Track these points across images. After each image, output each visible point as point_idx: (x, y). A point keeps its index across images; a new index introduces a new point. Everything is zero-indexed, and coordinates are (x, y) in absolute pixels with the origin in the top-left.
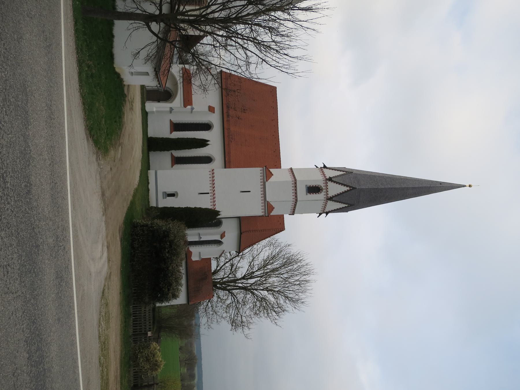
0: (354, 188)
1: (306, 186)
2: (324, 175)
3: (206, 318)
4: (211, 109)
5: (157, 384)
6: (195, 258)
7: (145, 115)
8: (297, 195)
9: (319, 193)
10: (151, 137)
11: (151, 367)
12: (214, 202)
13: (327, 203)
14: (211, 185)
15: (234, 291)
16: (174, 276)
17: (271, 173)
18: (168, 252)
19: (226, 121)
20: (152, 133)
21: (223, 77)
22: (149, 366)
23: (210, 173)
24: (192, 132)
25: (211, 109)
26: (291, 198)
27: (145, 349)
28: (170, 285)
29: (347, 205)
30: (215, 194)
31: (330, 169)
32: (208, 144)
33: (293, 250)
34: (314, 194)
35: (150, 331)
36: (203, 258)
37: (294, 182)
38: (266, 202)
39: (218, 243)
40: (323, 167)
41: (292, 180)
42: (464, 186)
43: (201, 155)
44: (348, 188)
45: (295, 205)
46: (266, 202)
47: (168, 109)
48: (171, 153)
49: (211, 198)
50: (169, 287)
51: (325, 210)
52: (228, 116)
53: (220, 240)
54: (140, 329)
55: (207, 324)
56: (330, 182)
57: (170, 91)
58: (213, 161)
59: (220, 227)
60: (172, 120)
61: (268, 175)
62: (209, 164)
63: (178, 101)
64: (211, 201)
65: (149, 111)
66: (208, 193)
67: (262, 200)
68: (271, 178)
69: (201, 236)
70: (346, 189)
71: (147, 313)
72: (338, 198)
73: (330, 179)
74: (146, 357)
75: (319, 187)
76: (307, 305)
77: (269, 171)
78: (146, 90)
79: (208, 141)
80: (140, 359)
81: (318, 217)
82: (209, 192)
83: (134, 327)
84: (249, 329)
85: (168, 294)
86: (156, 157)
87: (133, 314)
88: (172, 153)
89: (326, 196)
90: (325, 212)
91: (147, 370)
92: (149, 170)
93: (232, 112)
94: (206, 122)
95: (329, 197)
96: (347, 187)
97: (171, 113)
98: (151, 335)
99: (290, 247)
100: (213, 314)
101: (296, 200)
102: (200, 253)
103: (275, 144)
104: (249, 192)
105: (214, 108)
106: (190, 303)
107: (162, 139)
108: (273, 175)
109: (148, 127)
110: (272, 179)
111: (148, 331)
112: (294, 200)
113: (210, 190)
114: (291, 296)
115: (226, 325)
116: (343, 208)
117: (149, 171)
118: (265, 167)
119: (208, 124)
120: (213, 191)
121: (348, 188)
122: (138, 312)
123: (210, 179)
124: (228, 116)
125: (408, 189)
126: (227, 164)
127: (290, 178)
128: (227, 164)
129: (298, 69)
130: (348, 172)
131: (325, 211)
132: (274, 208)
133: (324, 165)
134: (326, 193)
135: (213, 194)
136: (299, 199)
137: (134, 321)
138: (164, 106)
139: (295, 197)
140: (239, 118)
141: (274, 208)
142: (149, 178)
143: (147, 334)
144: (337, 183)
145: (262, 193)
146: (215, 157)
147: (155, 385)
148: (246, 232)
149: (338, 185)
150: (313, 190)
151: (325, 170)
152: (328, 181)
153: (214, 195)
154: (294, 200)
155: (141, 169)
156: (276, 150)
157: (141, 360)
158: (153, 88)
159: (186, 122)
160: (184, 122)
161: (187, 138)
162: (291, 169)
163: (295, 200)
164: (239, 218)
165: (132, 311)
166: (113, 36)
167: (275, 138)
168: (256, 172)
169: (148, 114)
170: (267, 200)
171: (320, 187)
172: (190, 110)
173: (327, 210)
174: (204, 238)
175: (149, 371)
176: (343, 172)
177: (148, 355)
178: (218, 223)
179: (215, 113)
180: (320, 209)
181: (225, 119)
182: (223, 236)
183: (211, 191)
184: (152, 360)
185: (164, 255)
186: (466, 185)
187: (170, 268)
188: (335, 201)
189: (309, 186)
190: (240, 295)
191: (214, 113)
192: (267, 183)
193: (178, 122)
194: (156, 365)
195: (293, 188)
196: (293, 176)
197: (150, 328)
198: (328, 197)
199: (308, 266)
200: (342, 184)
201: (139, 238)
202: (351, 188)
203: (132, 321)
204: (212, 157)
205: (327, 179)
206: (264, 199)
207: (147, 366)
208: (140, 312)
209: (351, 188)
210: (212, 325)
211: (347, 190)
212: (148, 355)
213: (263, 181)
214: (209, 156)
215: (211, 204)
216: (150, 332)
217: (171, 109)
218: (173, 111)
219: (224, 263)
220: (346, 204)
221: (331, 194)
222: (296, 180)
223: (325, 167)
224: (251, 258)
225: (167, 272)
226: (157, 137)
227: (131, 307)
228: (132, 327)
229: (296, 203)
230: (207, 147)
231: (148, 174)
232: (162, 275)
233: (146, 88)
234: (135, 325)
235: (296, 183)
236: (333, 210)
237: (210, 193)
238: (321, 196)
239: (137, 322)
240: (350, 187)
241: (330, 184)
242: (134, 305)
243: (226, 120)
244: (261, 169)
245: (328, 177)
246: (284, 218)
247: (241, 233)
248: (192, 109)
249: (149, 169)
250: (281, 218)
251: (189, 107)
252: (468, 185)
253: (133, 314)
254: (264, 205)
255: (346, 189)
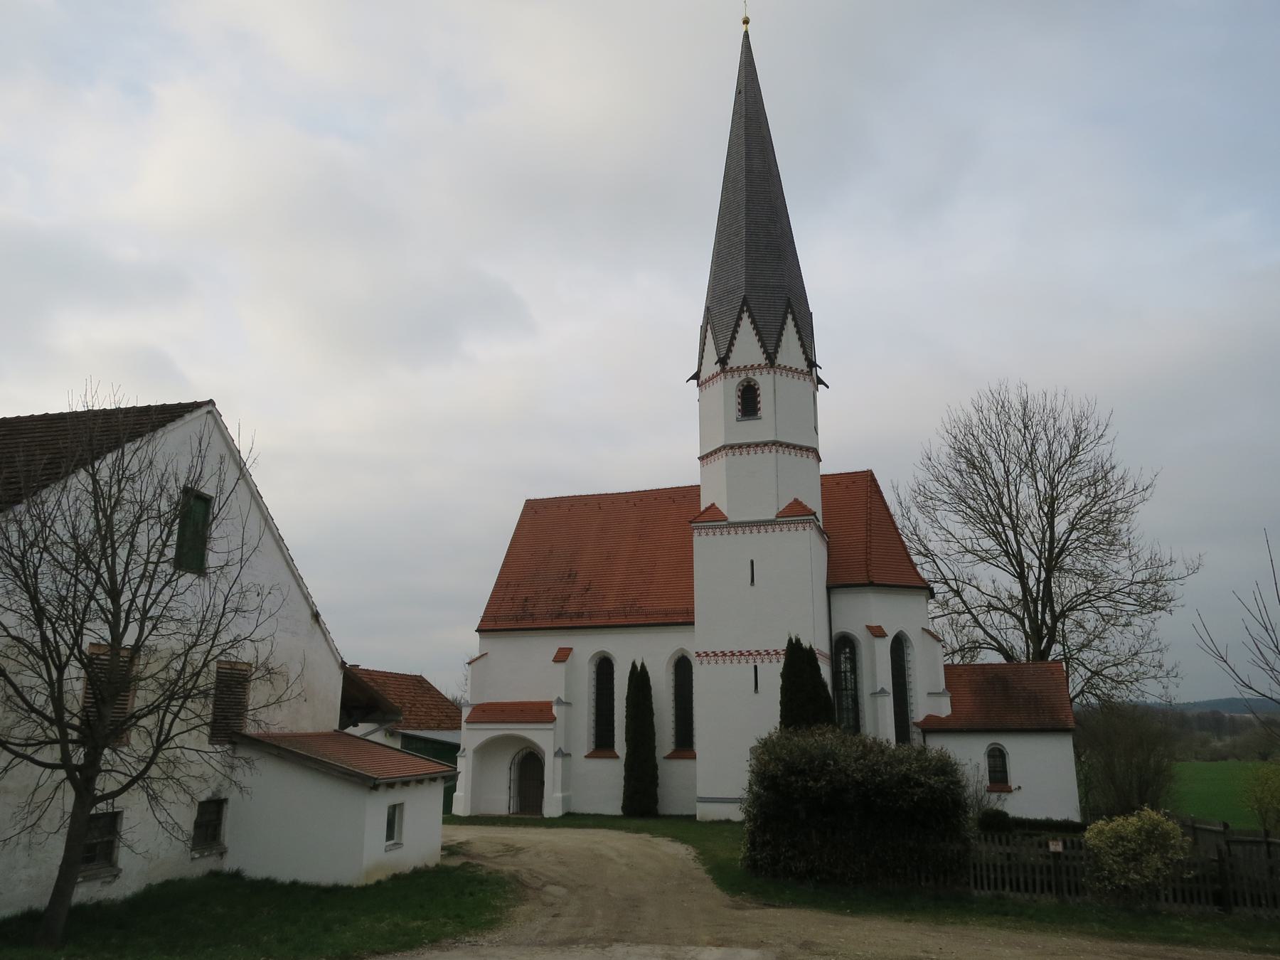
0: (745, 301)
1: (738, 420)
2: (714, 377)
3: (1146, 681)
4: (563, 656)
5: (1267, 834)
6: (944, 708)
7: (571, 819)
8: (754, 444)
9: (756, 387)
10: (623, 808)
11: (1156, 849)
12: (716, 655)
13: (782, 366)
14: (735, 661)
15: (1058, 609)
16: (882, 768)
17: (707, 509)
18: (816, 780)
19: (571, 621)
20: (612, 805)
21: (491, 625)
22: (1154, 853)
23: (705, 662)
24: (616, 703)
25: (563, 656)
26: (768, 456)
27: (1103, 864)
28: (906, 778)
29: (790, 317)
30: (741, 651)
31: (700, 364)
32: (643, 665)
33: (943, 451)
34: (758, 399)
35: (1047, 846)
36: (944, 687)
37: (730, 451)
38: (779, 520)
39: (899, 646)
40: (696, 381)
41: (724, 456)
42: (746, 35)
43: (672, 684)
44: (745, 316)
45: (788, 446)
46: (779, 520)
47: (559, 761)
48: (666, 760)
49: (767, 661)
50: (912, 783)
51: (802, 370)
52: (579, 615)
53: (889, 640)
54: (1041, 873)
55: (1163, 680)
56: (728, 361)
57: (521, 754)
58: (686, 655)
59: (857, 639)
60: (586, 754)
61: (713, 517)
62: (614, 662)
63: (542, 737)
64: (705, 662)
65: (561, 808)
66: (756, 667)
67: (774, 531)
68: (720, 509)
69: (878, 690)
70: (746, 322)
71: (1009, 851)
72: (770, 339)
73: (723, 361)
74: (1127, 861)
75: (741, 388)
76: (1093, 403)
77: (704, 511)
78: (517, 813)
79: (634, 665)
80: (1133, 880)
81: (828, 387)
82: (751, 665)
83: (1034, 891)
84: (1171, 561)
85: (931, 787)
86: (673, 798)
87: (996, 887)
88: (666, 755)
89: (765, 370)
90: (808, 370)
91: (1168, 861)
92: (695, 815)
93: (572, 607)
94: (593, 669)
95: (767, 361)
96: (741, 319)
97: (569, 755)
98: (1060, 844)
99: (934, 456)
100: (1141, 664)
101: (774, 443)
102: (929, 694)
103: (656, 499)
104: (752, 562)
105: (560, 649)
106: (1072, 725)
107: (628, 779)
108: (713, 505)
109: (601, 815)
110: (723, 507)
111: (1048, 851)
112: (774, 451)
113: (747, 662)
114: (1066, 449)
115: (1166, 625)
116: (796, 325)
117: (698, 819)
118: (693, 525)
119: (599, 663)
120: (751, 654)
121: (745, 316)
122: (992, 876)
123: (720, 661)
124: (579, 615)
125: (749, 171)
126: (685, 620)
127: (721, 462)
128: (685, 620)
129: (734, 457)
130: (708, 318)
131: (806, 369)
132: (796, 500)
133: (692, 378)
134: (756, 369)
135: (758, 657)
136: (771, 438)
137: (1018, 889)
138: (552, 770)
139: (766, 448)
140: (588, 590)
141: (796, 500)
142: (716, 818)
143: (1057, 855)
144: (731, 344)
145: (747, 531)
146: (677, 648)
147: (1270, 839)
148: (868, 572)
149: (736, 342)
150: (749, 402)
151: (703, 377)
152: (728, 368)
153: (760, 654)
154: (774, 451)
155: (672, 837)
156: (670, 498)
157: (1133, 876)
158: (512, 795)
159: (593, 717)
160: (593, 724)
161: (627, 717)
162: (701, 458)
163: (774, 447)
164: (830, 589)
165: (989, 892)
166: (294, 884)
167: (641, 500)
168: (706, 546)
169: (572, 811)
170: (772, 517)
171: (743, 385)
172: (563, 708)
173: (803, 365)
174: (885, 679)
175: (1169, 855)
176: (707, 330)
177: (1120, 855)
178: (844, 645)
179: (571, 647)
180: (805, 384)
181: (586, 622)
182: (877, 632)
183: (751, 661)
184: (1133, 845)
185: (823, 793)
186: (744, 30)
187: (858, 776)
188: (777, 345)
189: (740, 414)
190: (1068, 587)
191: (571, 649)
192: (732, 519)
193: (592, 739)
194: (1150, 834)
195: (745, 452)
196: (712, 455)
197: (1040, 845)
198: (766, 364)
199: (986, 404)
200: (735, 331)
201: (782, 857)
202: (745, 309)
203: (1019, 895)
204: (676, 657)
205: (723, 370)
206: (771, 525)
207: (1155, 860)
208: (991, 868)
209: (745, 309)
210: (1167, 666)
211: (749, 317)
212: (1120, 855)
213: (725, 529)
214: (672, 663)
215: (720, 661)
216: (1051, 843)
217: (560, 753)
218: (563, 750)
219: (978, 629)
220: (787, 318)
221: (759, 357)
222: (723, 446)
223: (696, 376)
224: (969, 557)
225: (869, 787)
226: (622, 791)
227: (976, 893)
228: (1035, 897)
229: (781, 444)
230: (648, 669)
231: (706, 822)
232: (879, 800)
233: (513, 813)
234: (1030, 888)
235: (732, 447)
236: (801, 350)
237: (755, 662)
238: (764, 382)
239: (1022, 880)
240: (741, 311)
241: (732, 363)
242: (972, 884)
243: (624, 620)
244: (696, 533)
245: (718, 368)
246: (841, 474)
247: (871, 585)
248: (559, 702)
249: (692, 818)
250: (832, 484)
251: (555, 710)
252: (744, 28)
253: (996, 887)
254: (785, 526)
255: (746, 322)
